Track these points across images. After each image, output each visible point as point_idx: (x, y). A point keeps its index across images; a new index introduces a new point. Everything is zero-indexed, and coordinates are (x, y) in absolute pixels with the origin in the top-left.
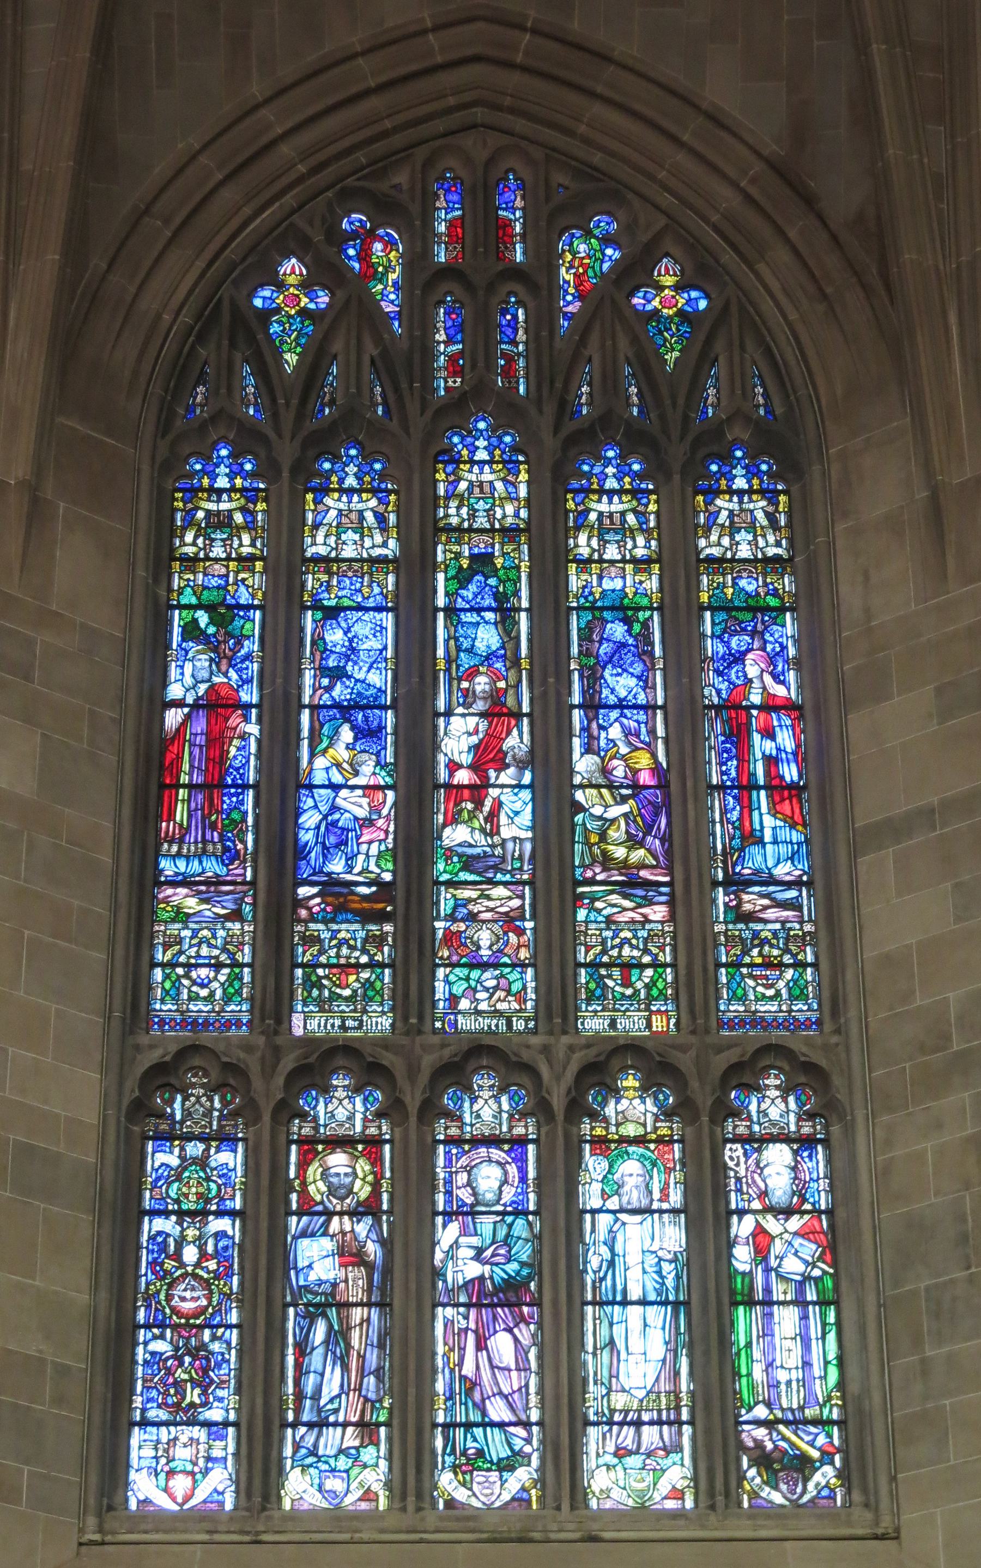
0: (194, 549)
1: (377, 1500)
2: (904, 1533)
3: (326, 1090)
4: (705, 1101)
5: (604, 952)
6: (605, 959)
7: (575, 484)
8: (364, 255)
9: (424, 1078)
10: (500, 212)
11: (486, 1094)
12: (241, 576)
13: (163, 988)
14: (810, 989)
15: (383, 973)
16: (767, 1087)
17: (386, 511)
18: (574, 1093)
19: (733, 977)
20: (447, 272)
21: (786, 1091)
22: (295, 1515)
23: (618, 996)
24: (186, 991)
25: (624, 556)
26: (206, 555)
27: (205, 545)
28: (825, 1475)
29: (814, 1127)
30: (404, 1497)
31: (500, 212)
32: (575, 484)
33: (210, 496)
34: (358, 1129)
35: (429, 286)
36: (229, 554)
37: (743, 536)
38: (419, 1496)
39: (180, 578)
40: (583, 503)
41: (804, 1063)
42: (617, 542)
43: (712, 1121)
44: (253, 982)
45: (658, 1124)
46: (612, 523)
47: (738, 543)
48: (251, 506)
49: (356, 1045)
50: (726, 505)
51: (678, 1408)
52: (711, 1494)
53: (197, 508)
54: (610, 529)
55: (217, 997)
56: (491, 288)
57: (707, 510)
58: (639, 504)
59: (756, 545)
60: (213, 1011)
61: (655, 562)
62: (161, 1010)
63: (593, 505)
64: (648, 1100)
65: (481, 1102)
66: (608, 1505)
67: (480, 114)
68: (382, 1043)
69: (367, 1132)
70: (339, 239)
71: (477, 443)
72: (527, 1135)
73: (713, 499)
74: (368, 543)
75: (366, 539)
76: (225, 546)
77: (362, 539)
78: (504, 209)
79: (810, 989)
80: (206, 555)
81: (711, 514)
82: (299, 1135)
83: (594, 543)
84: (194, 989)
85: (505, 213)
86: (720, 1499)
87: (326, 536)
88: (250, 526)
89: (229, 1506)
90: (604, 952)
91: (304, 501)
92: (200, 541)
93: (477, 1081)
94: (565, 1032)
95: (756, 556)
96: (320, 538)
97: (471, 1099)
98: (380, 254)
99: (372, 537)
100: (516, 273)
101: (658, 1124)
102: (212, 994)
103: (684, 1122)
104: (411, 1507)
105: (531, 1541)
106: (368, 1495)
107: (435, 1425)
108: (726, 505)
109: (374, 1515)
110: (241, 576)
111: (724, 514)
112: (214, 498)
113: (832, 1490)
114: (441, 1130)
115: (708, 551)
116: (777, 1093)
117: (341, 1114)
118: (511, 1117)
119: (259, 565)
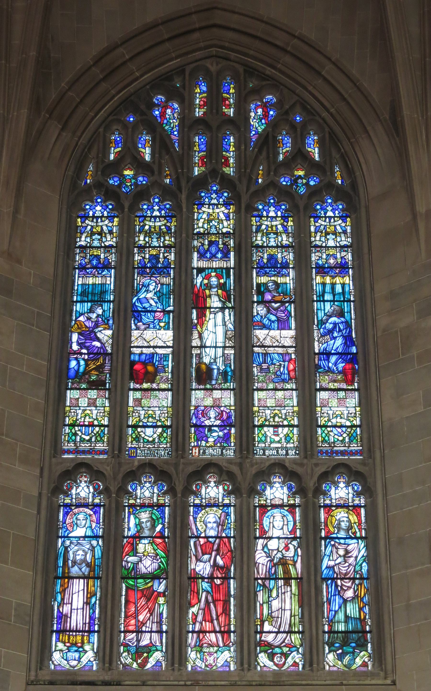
0: (321, 242)
1: (298, 667)
2: (397, 682)
3: (206, 482)
4: (244, 487)
5: (329, 420)
6: (330, 424)
7: (255, 213)
8: (163, 114)
9: (315, 478)
10: (224, 95)
11: (148, 485)
12: (166, 255)
13: (322, 437)
14: (106, 437)
15: (104, 429)
16: (275, 483)
17: (346, 225)
18: (317, 485)
19: (324, 432)
20: (199, 121)
21: (217, 484)
22: (330, 673)
23: (336, 440)
24: (332, 438)
25: (160, 245)
26: (150, 245)
27: (149, 240)
28: (157, 656)
29: (230, 500)
30: (173, 664)
31: (224, 95)
32: (139, 214)
33: (267, 219)
34: (155, 501)
35: (191, 128)
36: (277, 244)
37: (331, 237)
38: (180, 664)
39: (138, 256)
40: (143, 222)
41: (96, 470)
42: (274, 238)
43: (117, 495)
44: (171, 434)
45: (159, 498)
46: (272, 230)
47: (328, 239)
48: (285, 224)
49: (89, 462)
50: (90, 223)
51: (229, 625)
52: (242, 664)
53: (146, 225)
54: (271, 233)
55: (156, 441)
56: (219, 128)
57: (315, 225)
58: (168, 222)
59: (102, 241)
60: (154, 447)
61: (173, 247)
62: (322, 447)
63: (147, 223)
64: (285, 488)
65: (80, 488)
66: (335, 669)
67: (213, 50)
68: (230, 461)
69: (289, 503)
70: (152, 106)
71: (212, 196)
72: (165, 503)
73: (85, 220)
74: (339, 239)
75: (338, 237)
76: (158, 241)
77: (336, 237)
78: (225, 93)
79: (106, 437)
80: (150, 245)
81: (316, 227)
82: (194, 503)
83: (264, 239)
84: (83, 436)
85: (226, 95)
86: (246, 666)
87: (86, 237)
88: (111, 232)
89: (95, 668)
90: (329, 420)
91: (310, 222)
92: (147, 239)
93: (143, 479)
94: (183, 458)
95: (277, 244)
96: (83, 239)
97: (76, 487)
98: (169, 114)
99: (340, 236)
100: (229, 121)
101: (159, 498)
102: (154, 440)
103: (236, 498)
104: (176, 669)
105: (252, 685)
106: (295, 664)
107: (53, 631)
108: (323, 223)
109: (298, 674)
110: (166, 255)
111: (89, 227)
112: (153, 220)
113: (229, 662)
114: (193, 500)
115: (80, 243)
116: (279, 485)
117: (147, 494)
118: (94, 494)
119: (113, 250)
